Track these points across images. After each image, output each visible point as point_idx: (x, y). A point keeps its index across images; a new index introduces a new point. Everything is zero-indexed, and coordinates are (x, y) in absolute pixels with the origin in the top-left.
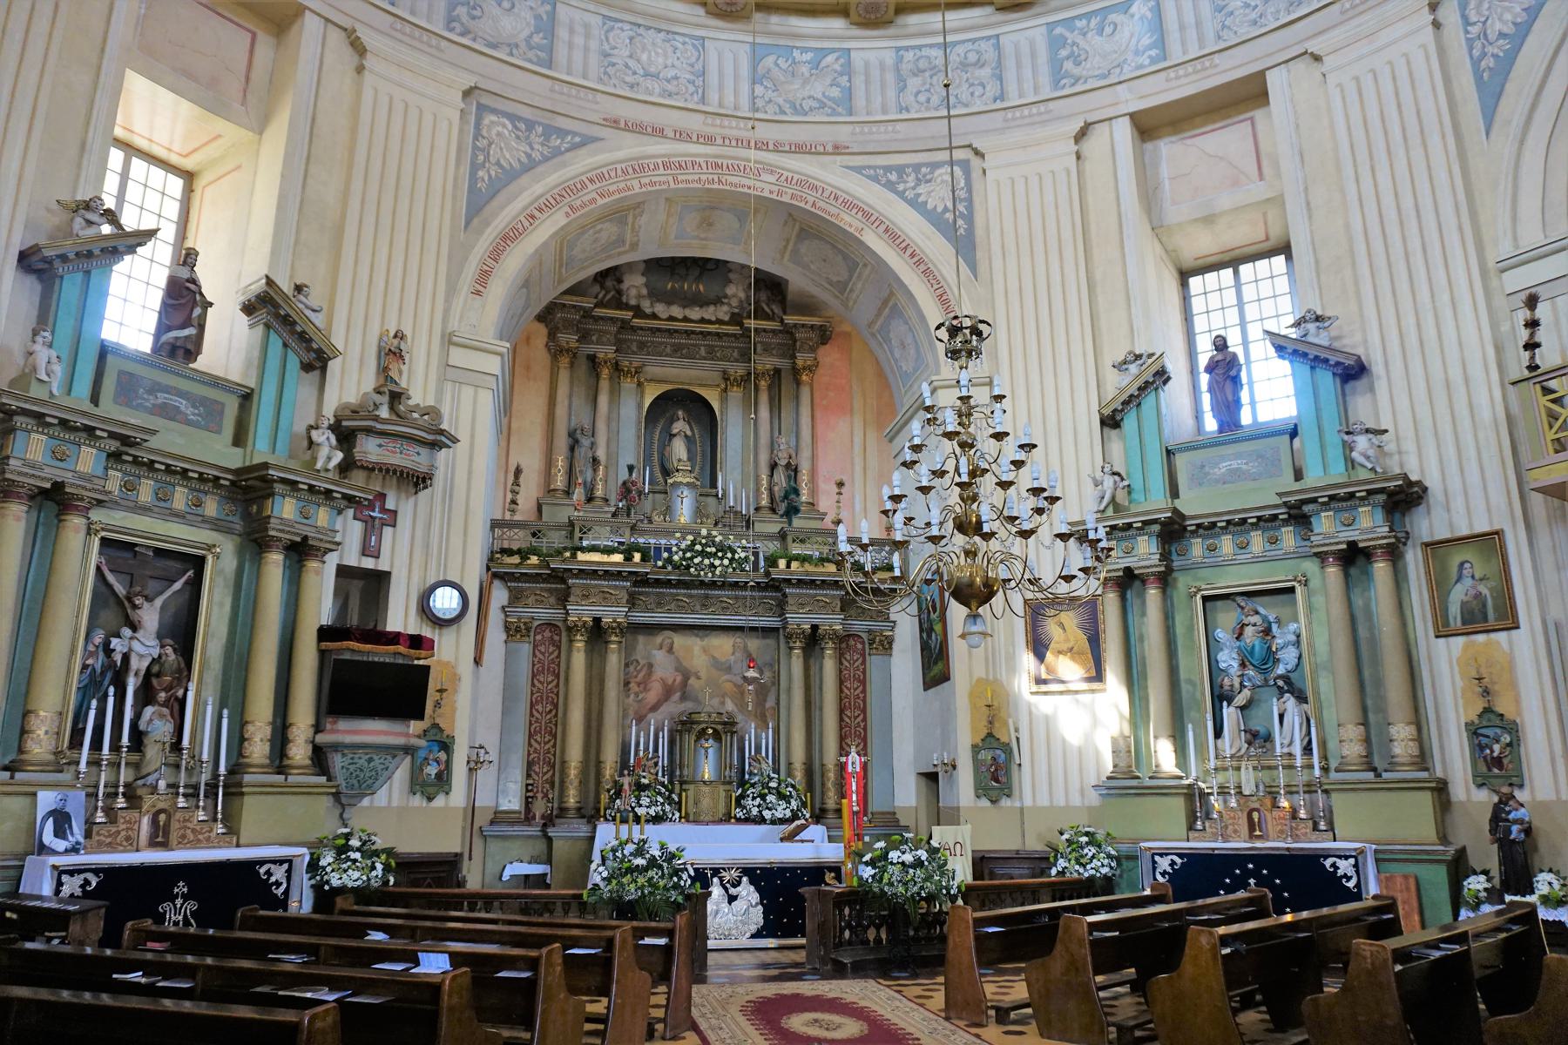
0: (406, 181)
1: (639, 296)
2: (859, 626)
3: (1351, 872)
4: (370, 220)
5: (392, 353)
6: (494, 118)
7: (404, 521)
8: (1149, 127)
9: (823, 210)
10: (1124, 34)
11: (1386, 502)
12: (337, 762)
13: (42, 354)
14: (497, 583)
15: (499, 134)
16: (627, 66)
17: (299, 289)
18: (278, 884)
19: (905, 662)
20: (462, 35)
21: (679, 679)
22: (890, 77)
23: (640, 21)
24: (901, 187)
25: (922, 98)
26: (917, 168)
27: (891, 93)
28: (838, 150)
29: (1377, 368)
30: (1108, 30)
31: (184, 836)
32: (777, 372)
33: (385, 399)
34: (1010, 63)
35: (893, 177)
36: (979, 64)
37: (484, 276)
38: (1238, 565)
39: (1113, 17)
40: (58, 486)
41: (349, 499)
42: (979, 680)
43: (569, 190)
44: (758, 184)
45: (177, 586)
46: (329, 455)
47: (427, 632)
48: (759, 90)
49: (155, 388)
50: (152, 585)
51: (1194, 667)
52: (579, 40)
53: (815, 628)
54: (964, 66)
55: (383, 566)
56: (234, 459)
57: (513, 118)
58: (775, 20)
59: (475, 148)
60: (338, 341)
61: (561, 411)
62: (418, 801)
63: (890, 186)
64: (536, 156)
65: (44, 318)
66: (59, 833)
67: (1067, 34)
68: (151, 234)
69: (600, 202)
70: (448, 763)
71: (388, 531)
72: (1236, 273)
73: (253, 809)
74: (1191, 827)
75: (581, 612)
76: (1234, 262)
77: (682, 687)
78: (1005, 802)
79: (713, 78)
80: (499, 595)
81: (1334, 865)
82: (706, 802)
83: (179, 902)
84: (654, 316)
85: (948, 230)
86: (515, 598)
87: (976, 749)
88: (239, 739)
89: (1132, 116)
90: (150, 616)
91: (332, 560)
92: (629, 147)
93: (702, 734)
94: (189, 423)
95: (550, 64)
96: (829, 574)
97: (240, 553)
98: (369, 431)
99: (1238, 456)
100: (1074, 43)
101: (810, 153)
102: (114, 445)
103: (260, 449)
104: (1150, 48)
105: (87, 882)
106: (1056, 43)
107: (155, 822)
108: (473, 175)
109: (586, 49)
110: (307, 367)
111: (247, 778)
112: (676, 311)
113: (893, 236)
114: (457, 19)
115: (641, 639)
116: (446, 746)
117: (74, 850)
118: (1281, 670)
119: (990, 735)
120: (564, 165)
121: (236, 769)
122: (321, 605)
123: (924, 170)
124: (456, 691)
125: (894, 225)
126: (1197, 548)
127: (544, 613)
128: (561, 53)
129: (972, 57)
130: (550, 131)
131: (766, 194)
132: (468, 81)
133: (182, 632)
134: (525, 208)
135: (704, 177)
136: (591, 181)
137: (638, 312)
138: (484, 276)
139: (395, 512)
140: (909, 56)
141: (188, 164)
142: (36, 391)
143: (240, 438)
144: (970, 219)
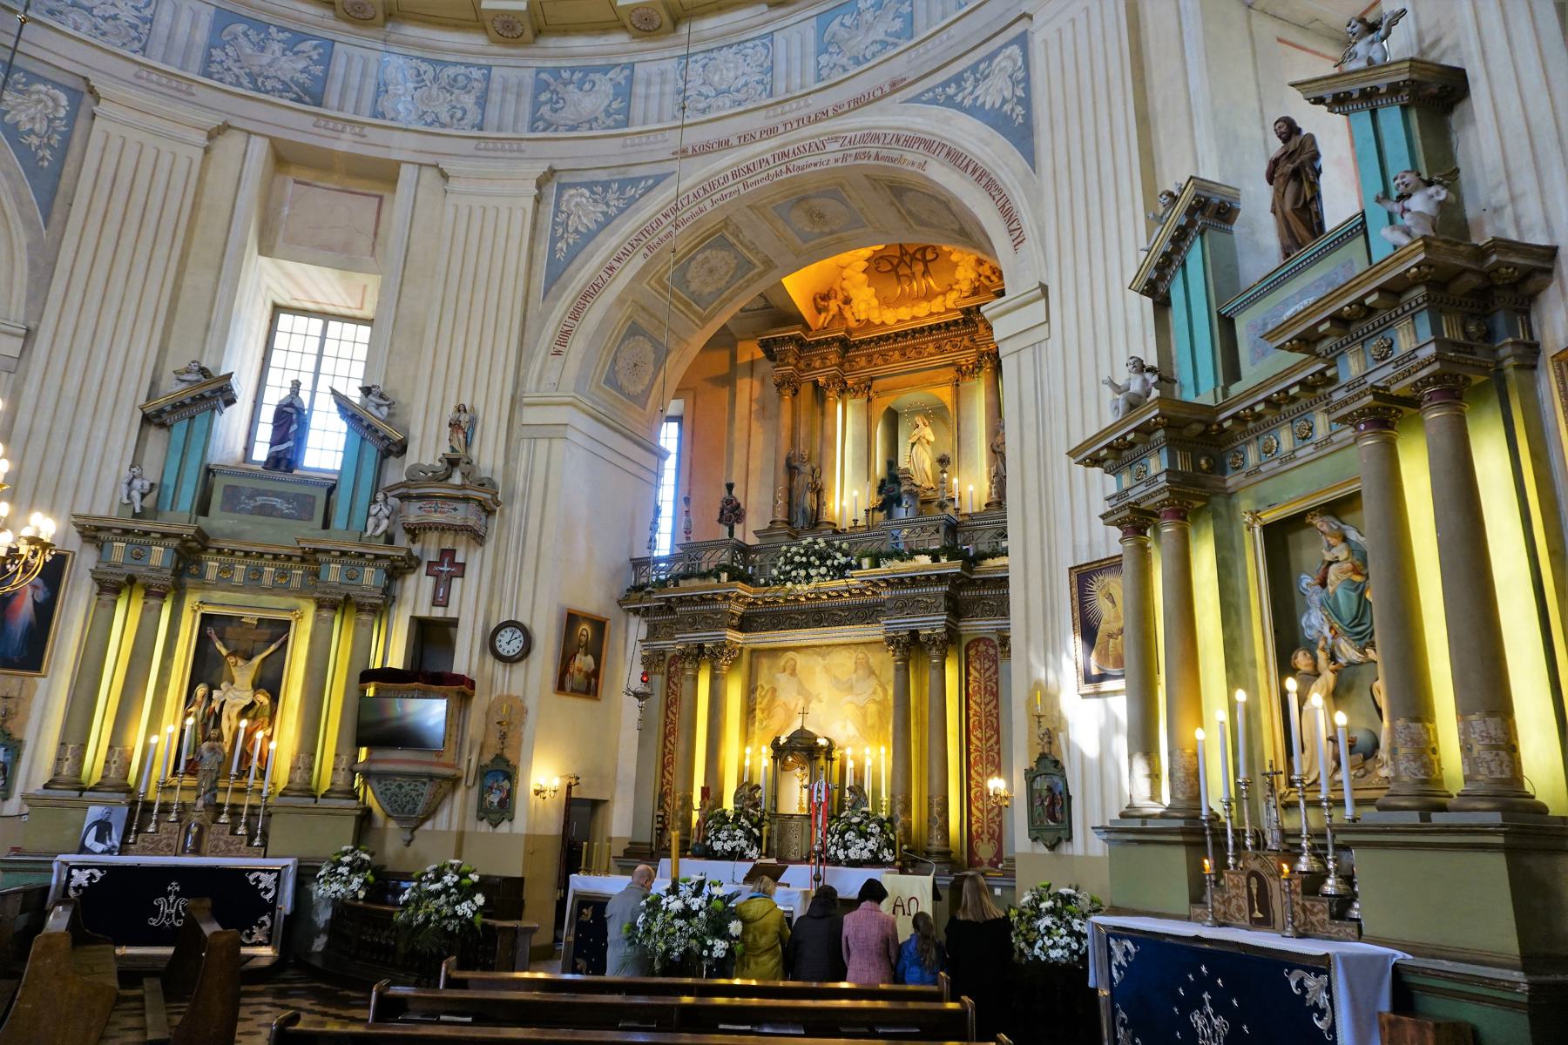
0: (483, 276)
1: (870, 308)
5: (463, 425)
6: (573, 192)
7: (472, 572)
11: (1428, 298)
15: (577, 204)
16: (700, 94)
18: (267, 890)
23: (713, 45)
26: (974, 68)
28: (896, 86)
29: (1474, 71)
35: (951, 90)
37: (564, 336)
43: (645, 231)
44: (824, 158)
48: (824, 59)
49: (255, 493)
55: (452, 613)
57: (589, 185)
59: (555, 223)
62: (484, 827)
63: (950, 102)
64: (612, 211)
66: (100, 838)
71: (457, 582)
74: (1197, 898)
76: (326, 316)
79: (781, 68)
81: (263, 923)
83: (171, 899)
85: (998, 120)
86: (653, 633)
92: (696, 172)
96: (925, 568)
101: (870, 103)
105: (92, 876)
113: (956, 158)
114: (542, 118)
117: (109, 852)
120: (638, 210)
124: (522, 723)
130: (624, 183)
131: (832, 164)
132: (541, 168)
134: (602, 264)
135: (772, 172)
136: (666, 216)
138: (564, 336)
139: (464, 565)
144: (1026, 102)
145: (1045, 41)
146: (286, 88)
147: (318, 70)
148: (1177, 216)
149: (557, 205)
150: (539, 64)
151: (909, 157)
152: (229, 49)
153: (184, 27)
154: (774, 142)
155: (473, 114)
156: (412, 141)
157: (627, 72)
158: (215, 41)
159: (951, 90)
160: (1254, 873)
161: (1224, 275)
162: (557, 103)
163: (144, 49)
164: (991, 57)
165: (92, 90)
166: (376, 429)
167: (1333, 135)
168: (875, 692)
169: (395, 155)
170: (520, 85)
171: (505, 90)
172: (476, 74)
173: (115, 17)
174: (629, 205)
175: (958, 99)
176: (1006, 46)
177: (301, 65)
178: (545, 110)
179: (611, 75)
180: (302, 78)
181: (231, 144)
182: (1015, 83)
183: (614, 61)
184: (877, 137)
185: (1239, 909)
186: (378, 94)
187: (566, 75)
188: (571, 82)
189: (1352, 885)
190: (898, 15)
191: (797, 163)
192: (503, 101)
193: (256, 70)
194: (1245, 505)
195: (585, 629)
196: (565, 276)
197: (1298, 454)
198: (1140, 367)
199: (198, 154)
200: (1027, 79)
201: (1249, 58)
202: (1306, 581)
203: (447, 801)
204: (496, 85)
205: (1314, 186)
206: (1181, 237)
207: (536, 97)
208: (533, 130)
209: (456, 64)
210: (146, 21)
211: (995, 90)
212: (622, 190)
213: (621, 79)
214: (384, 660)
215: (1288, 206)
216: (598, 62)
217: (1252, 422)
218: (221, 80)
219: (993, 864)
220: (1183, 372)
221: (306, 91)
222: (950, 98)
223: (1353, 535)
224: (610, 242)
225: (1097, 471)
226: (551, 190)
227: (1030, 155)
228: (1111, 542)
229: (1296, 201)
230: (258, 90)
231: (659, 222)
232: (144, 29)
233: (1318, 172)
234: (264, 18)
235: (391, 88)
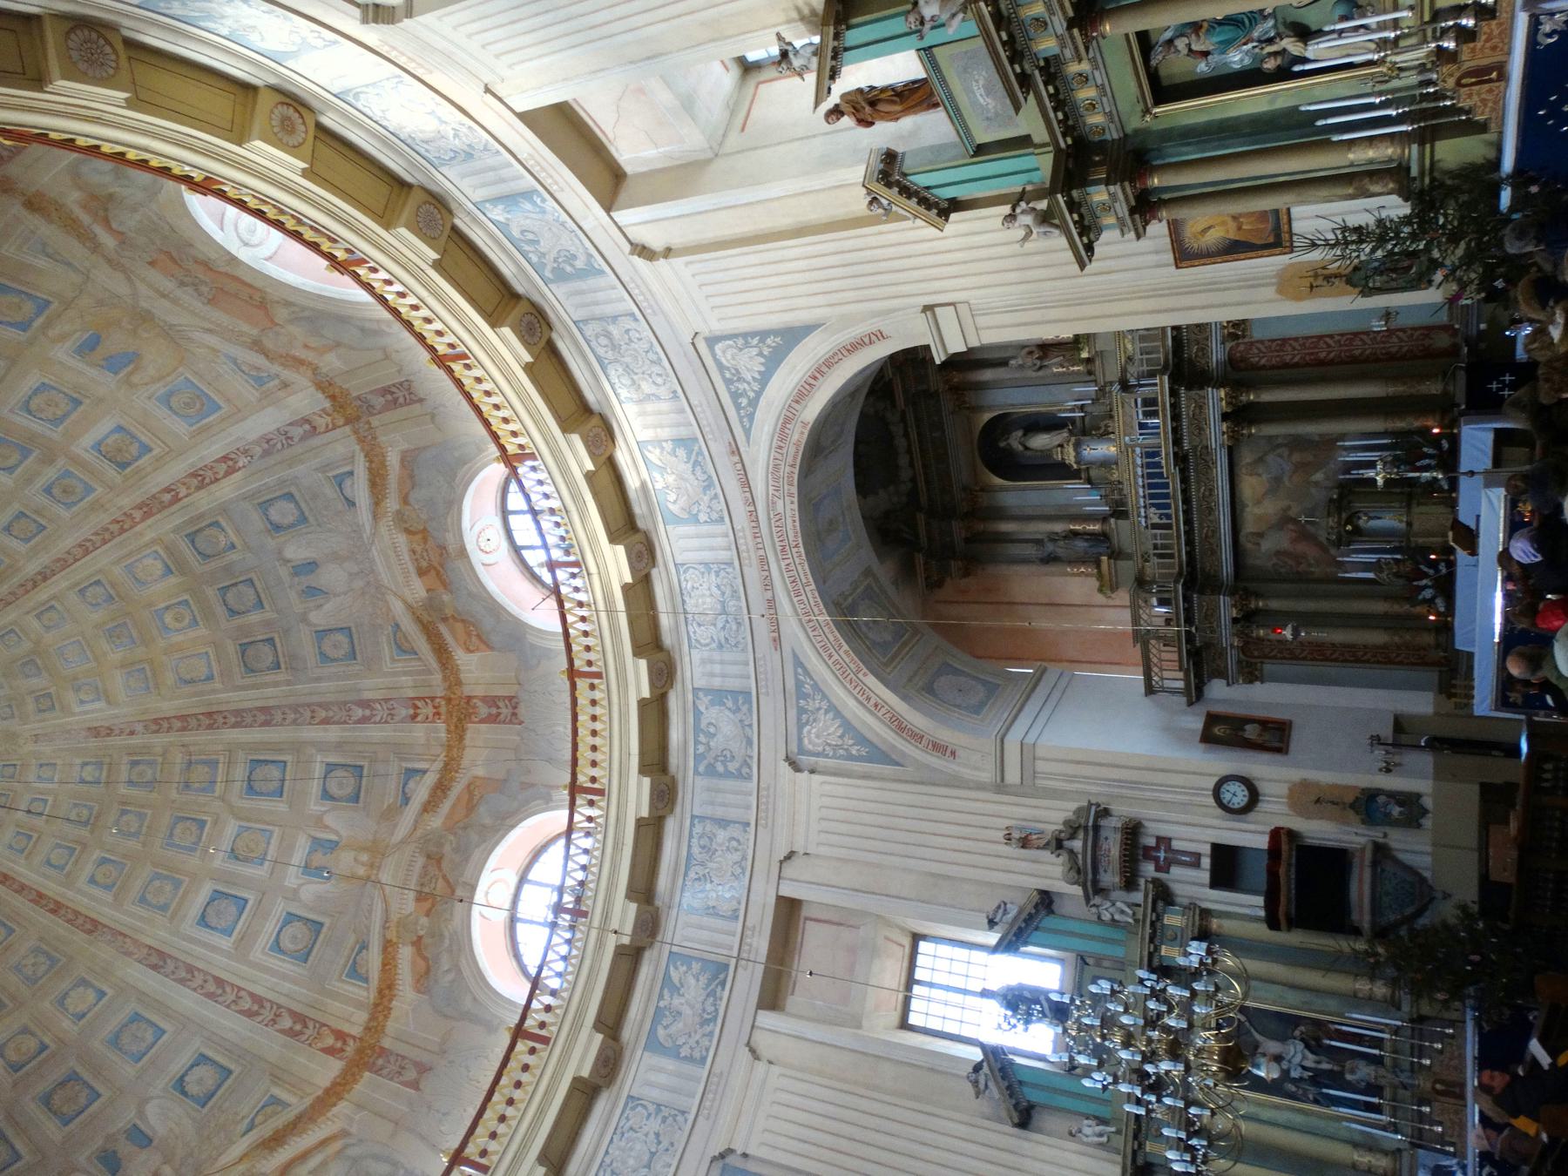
6: (806, 741)
9: (795, 458)
15: (818, 737)
16: (723, 628)
20: (750, 768)
21: (1291, 527)
24: (752, 395)
26: (728, 382)
28: (736, 451)
31: (1455, 1068)
35: (744, 401)
36: (608, 335)
37: (938, 748)
42: (1279, 291)
44: (789, 513)
55: (1206, 849)
62: (1427, 822)
63: (754, 403)
64: (824, 705)
67: (549, 267)
69: (846, 647)
71: (1176, 845)
72: (919, 982)
76: (910, 981)
84: (913, 480)
85: (774, 361)
86: (1221, 674)
89: (608, 209)
92: (791, 627)
99: (969, 91)
100: (555, 260)
104: (534, 204)
112: (903, 461)
113: (801, 395)
114: (739, 770)
123: (728, 375)
129: (603, 341)
130: (801, 695)
131: (796, 506)
132: (785, 767)
136: (830, 656)
138: (938, 748)
139: (1159, 839)
141: (907, 941)
144: (763, 335)
145: (720, 319)
146: (712, 994)
147: (696, 966)
148: (888, 195)
149: (818, 755)
150: (691, 773)
151: (796, 437)
152: (680, 1042)
153: (662, 1079)
154: (772, 559)
155: (734, 831)
156: (759, 885)
157: (701, 694)
158: (674, 1053)
159: (744, 401)
160: (1459, 84)
161: (936, 157)
162: (725, 756)
163: (683, 1113)
165: (722, 1156)
166: (1026, 923)
167: (862, 73)
168: (1280, 456)
169: (772, 901)
170: (709, 790)
171: (712, 803)
172: (698, 829)
173: (657, 1135)
174: (820, 690)
175: (752, 395)
176: (714, 355)
177: (692, 981)
178: (732, 767)
179: (702, 708)
180: (703, 980)
181: (761, 1040)
182: (747, 345)
184: (776, 466)
185: (1490, 91)
186: (717, 915)
187: (701, 749)
188: (708, 744)
189: (1467, 6)
191: (791, 538)
192: (724, 805)
193: (697, 1019)
194: (1135, 123)
195: (1218, 731)
196: (884, 748)
197: (1099, 82)
198: (1011, 217)
199: (775, 1069)
200: (746, 335)
201: (759, 152)
202: (1202, 67)
203: (1401, 856)
205: (884, 90)
206: (906, 191)
207: (720, 775)
208: (749, 777)
209: (690, 846)
210: (659, 1110)
211: (749, 363)
212: (805, 696)
213: (706, 700)
214: (1255, 919)
215: (898, 108)
216: (691, 720)
217: (1071, 124)
218: (707, 1050)
219: (1455, 332)
220: (1014, 185)
221: (715, 977)
222: (750, 404)
223: (1168, 35)
224: (851, 707)
225: (1098, 249)
226: (804, 760)
227: (807, 329)
228: (1158, 229)
229: (894, 102)
230: (715, 1018)
231: (836, 663)
232: (665, 1112)
233: (872, 88)
234: (652, 1011)
235: (711, 904)
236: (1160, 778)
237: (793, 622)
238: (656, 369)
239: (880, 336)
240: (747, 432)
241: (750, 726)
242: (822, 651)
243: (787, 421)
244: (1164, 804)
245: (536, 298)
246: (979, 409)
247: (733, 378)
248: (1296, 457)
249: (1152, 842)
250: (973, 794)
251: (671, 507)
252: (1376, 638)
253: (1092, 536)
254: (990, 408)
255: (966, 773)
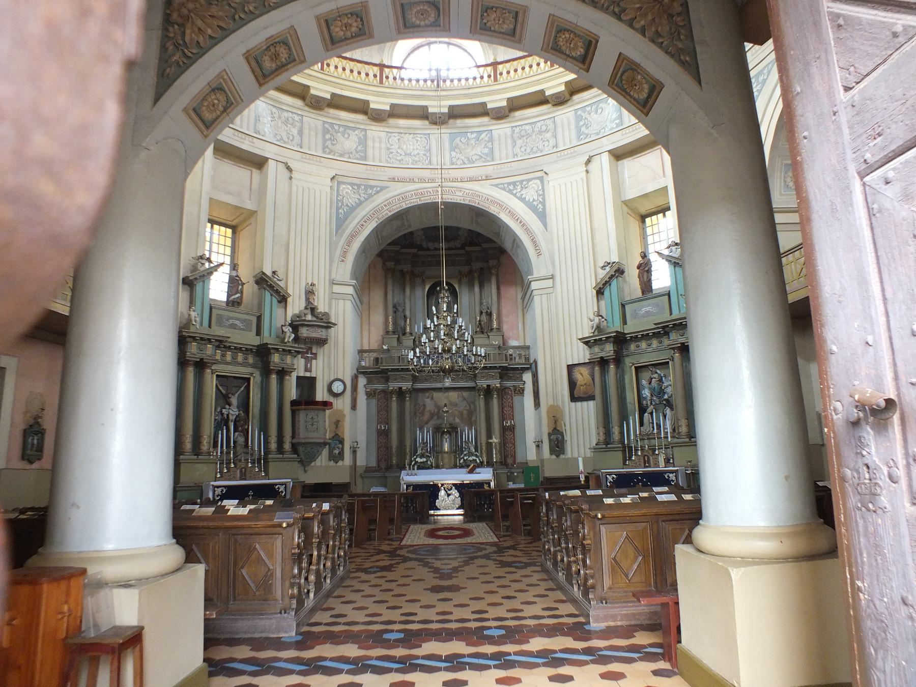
2: (509, 384)
3: (674, 478)
4: (299, 239)
5: (310, 292)
8: (619, 155)
10: (606, 112)
12: (301, 449)
13: (193, 314)
14: (360, 376)
17: (274, 273)
19: (528, 399)
20: (329, 153)
22: (509, 141)
24: (514, 192)
25: (523, 149)
26: (521, 182)
27: (510, 148)
28: (487, 178)
30: (599, 111)
32: (482, 269)
33: (309, 311)
34: (559, 130)
35: (511, 187)
36: (547, 131)
37: (344, 254)
38: (648, 352)
39: (601, 105)
40: (202, 359)
41: (298, 352)
43: (376, 211)
45: (242, 389)
46: (290, 336)
47: (331, 399)
50: (234, 389)
51: (631, 397)
52: (377, 145)
53: (488, 386)
54: (540, 132)
56: (256, 341)
57: (352, 184)
58: (459, 122)
60: (290, 291)
61: (390, 297)
62: (332, 463)
63: (510, 192)
64: (362, 199)
65: (192, 302)
68: (222, 264)
69: (390, 214)
70: (343, 449)
73: (272, 466)
74: (624, 464)
75: (393, 385)
77: (437, 413)
78: (562, 456)
80: (362, 381)
82: (446, 461)
84: (428, 249)
85: (533, 208)
86: (369, 382)
87: (550, 435)
88: (267, 443)
89: (609, 151)
90: (234, 400)
91: (294, 375)
92: (400, 188)
93: (443, 433)
94: (243, 330)
95: (365, 158)
97: (261, 374)
98: (303, 325)
99: (649, 305)
102: (217, 343)
103: (268, 337)
104: (615, 119)
106: (578, 118)
107: (241, 472)
108: (337, 212)
109: (380, 148)
110: (280, 302)
111: (270, 456)
113: (512, 214)
115: (420, 394)
116: (342, 442)
118: (666, 397)
119: (555, 429)
121: (266, 453)
122: (292, 392)
125: (512, 210)
126: (633, 347)
127: (380, 387)
128: (370, 152)
129: (544, 128)
131: (458, 201)
133: (245, 405)
137: (420, 248)
138: (344, 254)
139: (316, 354)
140: (517, 130)
141: (233, 223)
142: (192, 329)
143: (259, 333)
150: (324, 119)
151: (493, 208)
164: (529, 180)
174: (369, 197)
178: (328, 143)
179: (356, 132)
182: (539, 195)
183: (358, 126)
186: (256, 120)
190: (486, 147)
192: (309, 134)
200: (543, 195)
204: (306, 126)
206: (611, 277)
207: (324, 136)
211: (530, 194)
212: (366, 189)
227: (545, 224)
236: (340, 356)
237: (403, 190)
238: (528, 150)
239: (539, 254)
240: (496, 186)
241: (349, 158)
242: (387, 202)
243: (500, 205)
244: (329, 357)
245: (569, 103)
246: (460, 283)
247: (523, 184)
248: (465, 412)
249: (314, 351)
250: (328, 267)
251: (458, 139)
252: (394, 443)
253: (405, 329)
254: (460, 288)
255: (335, 266)
